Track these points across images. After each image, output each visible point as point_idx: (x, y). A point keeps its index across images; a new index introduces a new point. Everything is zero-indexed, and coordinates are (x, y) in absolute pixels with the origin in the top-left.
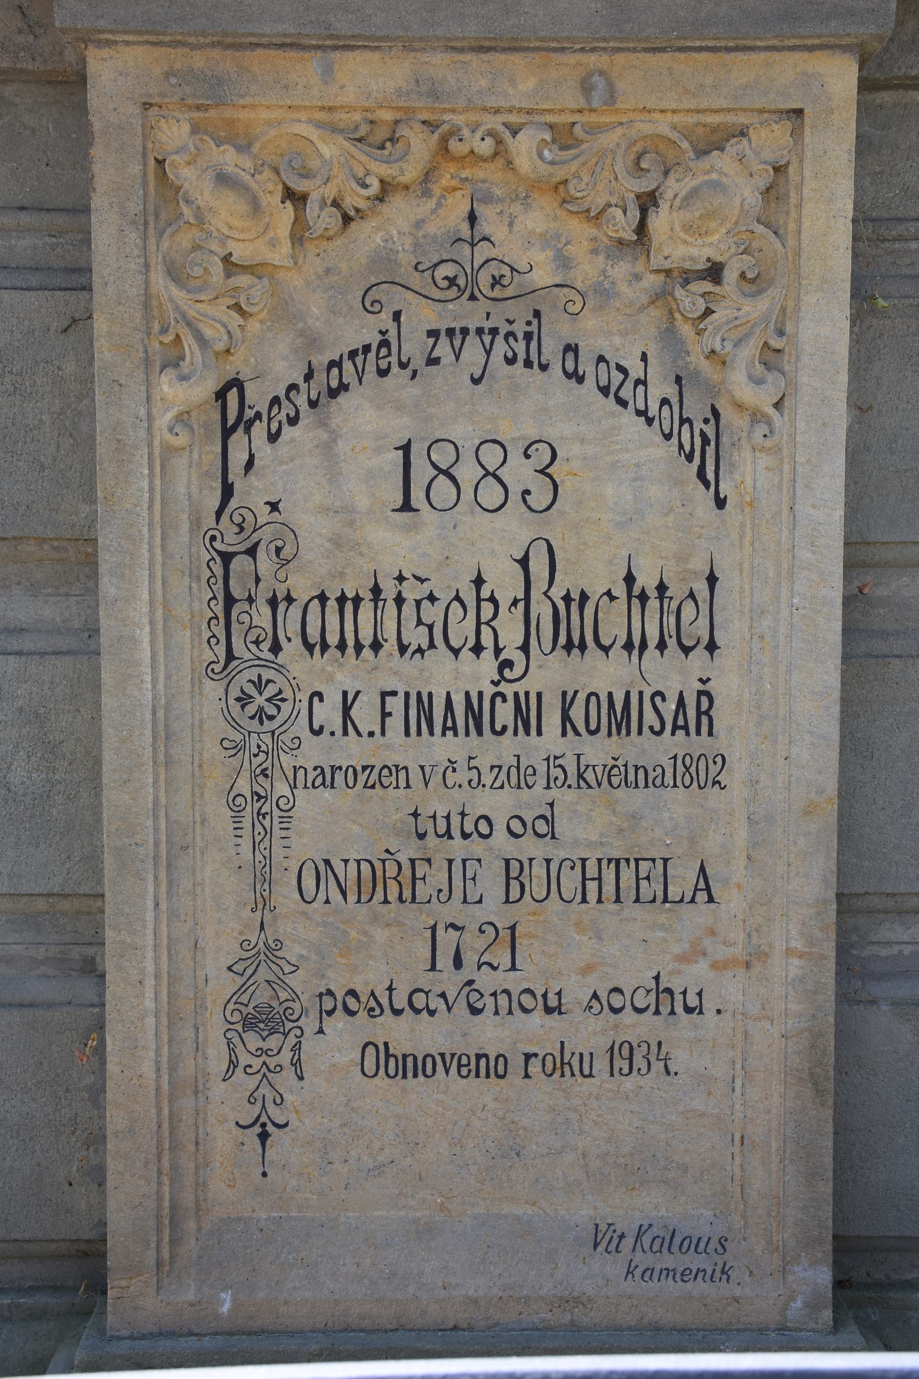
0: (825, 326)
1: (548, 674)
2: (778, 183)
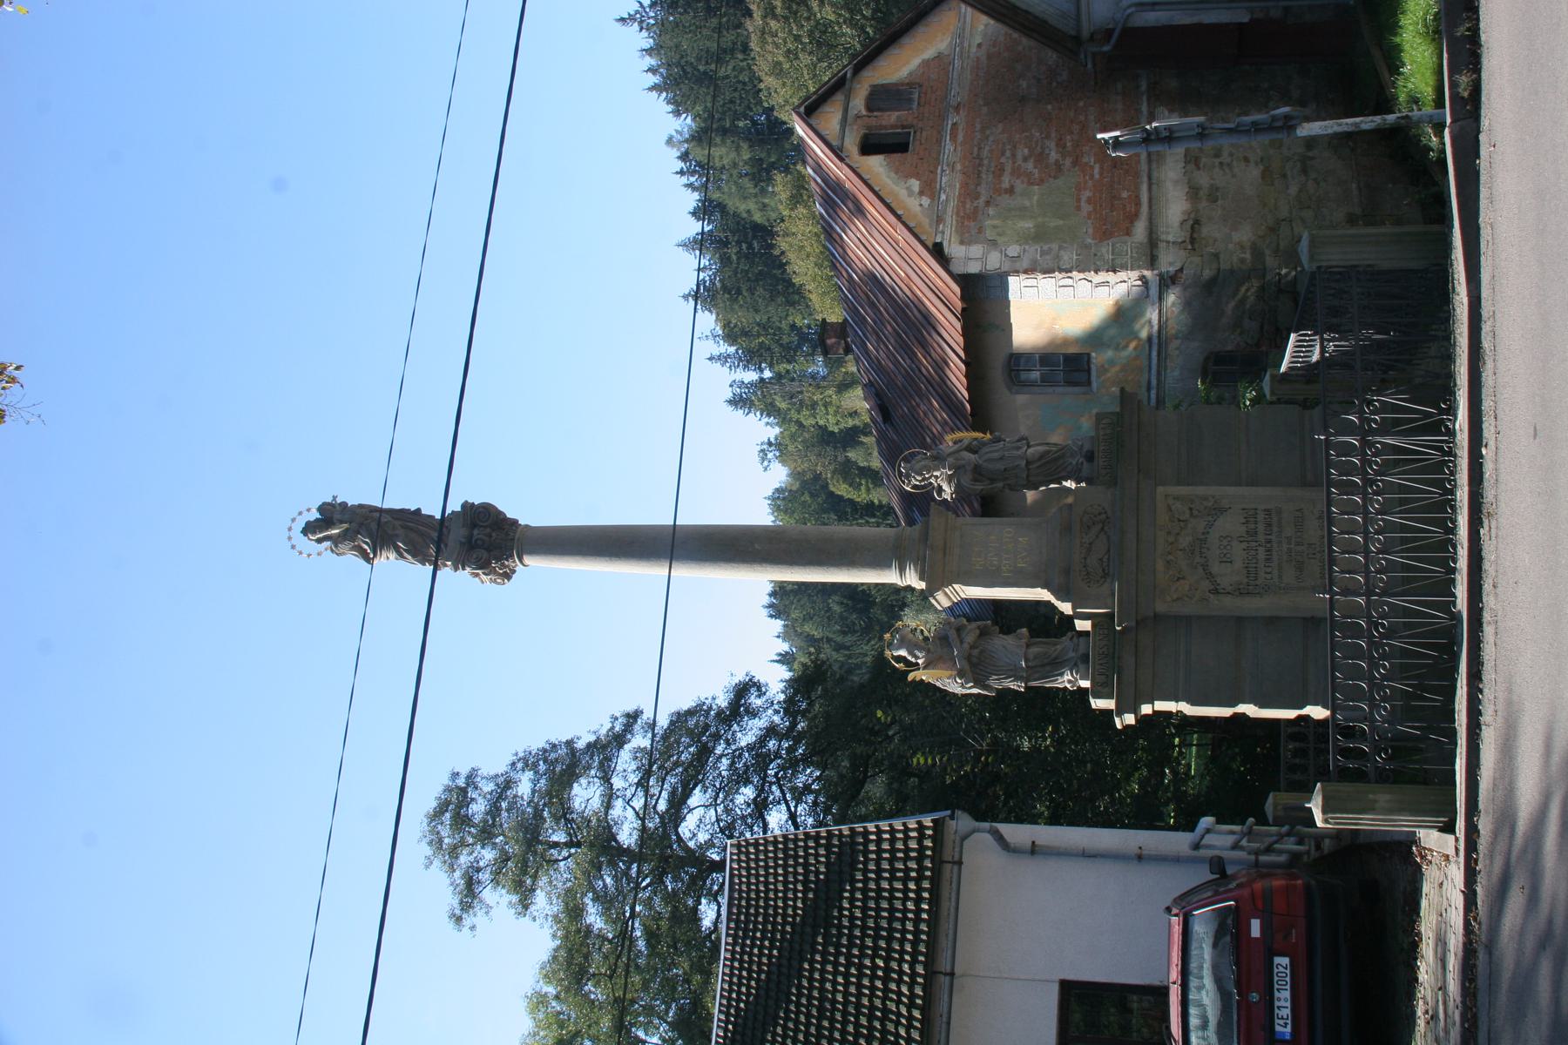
0: (1200, 490)
1: (1261, 538)
2: (1176, 498)
